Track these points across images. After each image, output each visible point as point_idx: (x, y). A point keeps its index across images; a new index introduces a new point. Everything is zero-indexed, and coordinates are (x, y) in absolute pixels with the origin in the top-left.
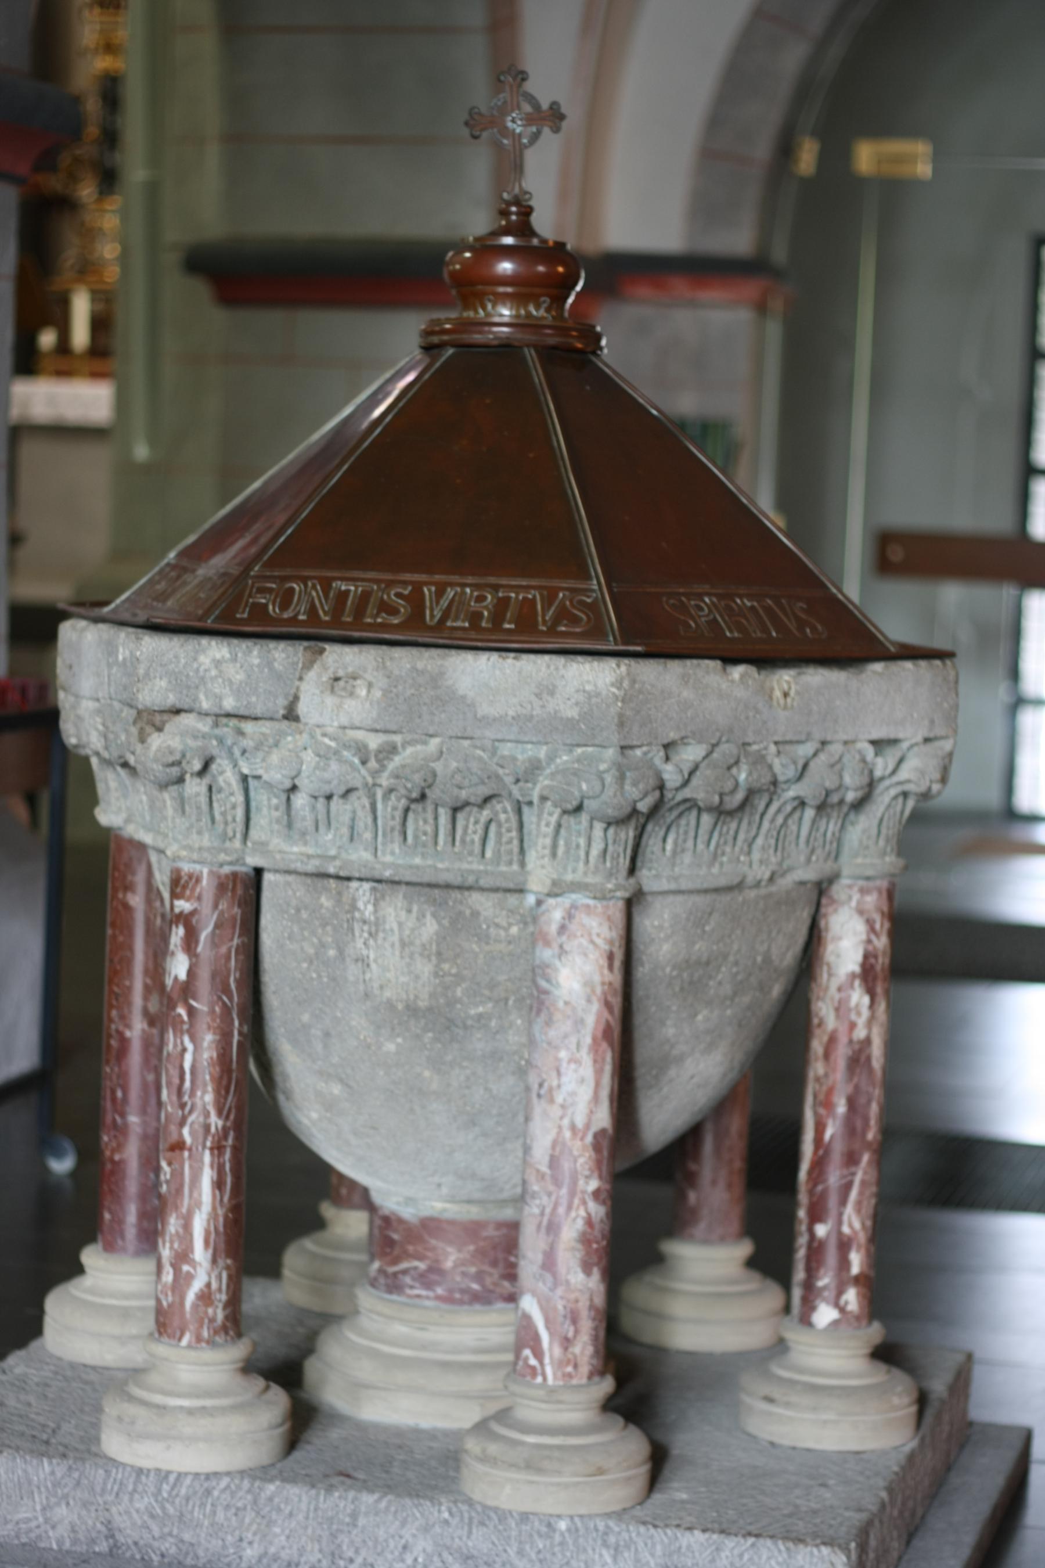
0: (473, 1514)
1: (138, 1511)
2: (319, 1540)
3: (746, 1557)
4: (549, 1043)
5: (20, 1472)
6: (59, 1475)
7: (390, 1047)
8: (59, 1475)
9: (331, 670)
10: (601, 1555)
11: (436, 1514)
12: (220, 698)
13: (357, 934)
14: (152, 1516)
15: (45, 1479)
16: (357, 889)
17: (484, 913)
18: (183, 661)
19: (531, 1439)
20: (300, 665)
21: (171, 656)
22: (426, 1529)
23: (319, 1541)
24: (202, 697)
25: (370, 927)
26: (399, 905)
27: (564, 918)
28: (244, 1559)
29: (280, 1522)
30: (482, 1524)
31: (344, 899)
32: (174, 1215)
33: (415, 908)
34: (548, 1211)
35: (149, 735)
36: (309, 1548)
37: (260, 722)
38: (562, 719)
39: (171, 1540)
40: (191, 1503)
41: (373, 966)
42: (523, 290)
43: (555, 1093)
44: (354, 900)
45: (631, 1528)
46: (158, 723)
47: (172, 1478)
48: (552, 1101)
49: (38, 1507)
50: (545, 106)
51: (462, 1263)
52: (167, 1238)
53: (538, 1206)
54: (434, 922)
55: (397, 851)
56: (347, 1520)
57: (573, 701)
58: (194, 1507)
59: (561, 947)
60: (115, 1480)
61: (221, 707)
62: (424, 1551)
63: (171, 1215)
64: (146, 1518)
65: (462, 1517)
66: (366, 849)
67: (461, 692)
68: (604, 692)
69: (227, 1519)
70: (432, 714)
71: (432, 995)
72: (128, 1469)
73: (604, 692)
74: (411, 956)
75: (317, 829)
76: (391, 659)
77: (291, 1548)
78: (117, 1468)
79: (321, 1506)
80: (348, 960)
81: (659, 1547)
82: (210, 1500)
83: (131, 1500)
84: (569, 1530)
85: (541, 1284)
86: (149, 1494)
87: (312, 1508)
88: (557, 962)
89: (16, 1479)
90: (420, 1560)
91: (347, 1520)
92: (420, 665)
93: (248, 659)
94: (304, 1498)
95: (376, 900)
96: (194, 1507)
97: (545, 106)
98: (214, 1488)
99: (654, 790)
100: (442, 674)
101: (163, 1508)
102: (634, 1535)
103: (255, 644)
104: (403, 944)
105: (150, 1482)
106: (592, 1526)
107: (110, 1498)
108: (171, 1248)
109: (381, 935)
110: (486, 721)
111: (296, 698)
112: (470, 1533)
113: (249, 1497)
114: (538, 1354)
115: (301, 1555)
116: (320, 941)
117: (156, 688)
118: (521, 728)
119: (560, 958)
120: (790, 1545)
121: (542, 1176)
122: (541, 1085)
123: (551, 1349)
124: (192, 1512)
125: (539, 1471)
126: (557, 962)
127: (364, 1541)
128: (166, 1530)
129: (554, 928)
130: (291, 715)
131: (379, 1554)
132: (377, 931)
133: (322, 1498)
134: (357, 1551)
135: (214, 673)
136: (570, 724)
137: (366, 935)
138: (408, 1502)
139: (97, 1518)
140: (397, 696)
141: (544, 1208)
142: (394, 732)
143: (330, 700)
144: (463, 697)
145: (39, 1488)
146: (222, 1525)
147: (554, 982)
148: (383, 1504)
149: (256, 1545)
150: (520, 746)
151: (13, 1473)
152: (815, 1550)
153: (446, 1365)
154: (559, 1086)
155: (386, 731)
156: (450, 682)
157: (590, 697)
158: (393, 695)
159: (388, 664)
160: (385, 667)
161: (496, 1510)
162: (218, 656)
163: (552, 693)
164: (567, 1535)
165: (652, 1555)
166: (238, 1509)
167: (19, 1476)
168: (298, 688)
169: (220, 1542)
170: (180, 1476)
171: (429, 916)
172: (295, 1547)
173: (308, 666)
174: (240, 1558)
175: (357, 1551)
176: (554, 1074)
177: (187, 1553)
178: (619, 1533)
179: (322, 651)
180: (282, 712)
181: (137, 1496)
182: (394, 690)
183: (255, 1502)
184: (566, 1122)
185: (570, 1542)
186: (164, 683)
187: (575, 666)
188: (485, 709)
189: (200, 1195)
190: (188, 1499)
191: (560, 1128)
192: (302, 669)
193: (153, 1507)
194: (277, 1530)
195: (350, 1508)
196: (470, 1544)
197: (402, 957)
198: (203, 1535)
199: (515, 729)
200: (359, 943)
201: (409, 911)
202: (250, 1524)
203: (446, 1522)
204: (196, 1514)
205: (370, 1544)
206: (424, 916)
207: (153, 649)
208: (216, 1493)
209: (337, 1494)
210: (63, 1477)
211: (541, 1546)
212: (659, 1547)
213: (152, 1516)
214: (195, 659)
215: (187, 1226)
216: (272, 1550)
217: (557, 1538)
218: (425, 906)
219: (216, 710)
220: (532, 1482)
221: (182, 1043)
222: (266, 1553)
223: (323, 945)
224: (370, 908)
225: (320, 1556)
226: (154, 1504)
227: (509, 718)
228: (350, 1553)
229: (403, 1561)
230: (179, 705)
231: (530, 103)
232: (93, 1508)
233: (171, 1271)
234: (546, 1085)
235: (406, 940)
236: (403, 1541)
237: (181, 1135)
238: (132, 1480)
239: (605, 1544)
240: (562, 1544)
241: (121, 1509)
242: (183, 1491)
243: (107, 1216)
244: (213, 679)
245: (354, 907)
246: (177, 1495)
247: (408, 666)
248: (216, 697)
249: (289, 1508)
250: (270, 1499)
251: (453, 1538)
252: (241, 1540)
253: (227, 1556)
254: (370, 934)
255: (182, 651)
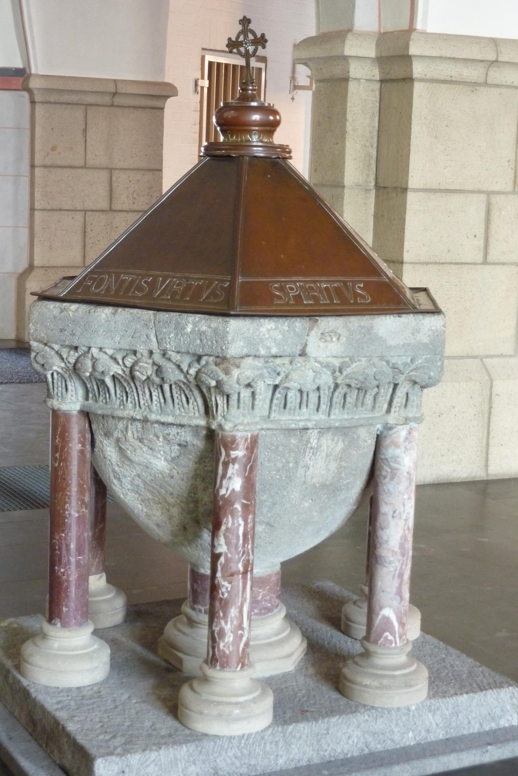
0: (378, 713)
1: (229, 757)
2: (312, 745)
3: (482, 699)
4: (399, 492)
5: (172, 756)
6: (191, 751)
7: (307, 505)
8: (191, 751)
9: (322, 329)
10: (428, 716)
11: (362, 718)
12: (269, 348)
13: (307, 454)
14: (236, 757)
15: (184, 755)
16: (311, 433)
17: (362, 436)
18: (251, 331)
19: (397, 673)
20: (308, 329)
21: (245, 329)
22: (358, 726)
23: (312, 746)
24: (261, 349)
25: (314, 450)
26: (329, 438)
27: (407, 434)
28: (279, 764)
29: (295, 742)
30: (382, 717)
31: (304, 439)
32: (234, 608)
33: (336, 438)
34: (398, 568)
35: (232, 370)
36: (308, 751)
37: (283, 358)
38: (422, 343)
39: (245, 766)
40: (255, 745)
41: (311, 468)
42: (247, 128)
43: (402, 515)
44: (309, 438)
45: (440, 700)
46: (238, 364)
47: (245, 737)
48: (401, 518)
49: (180, 770)
50: (259, 36)
51: (264, 596)
52: (229, 619)
53: (393, 567)
54: (342, 443)
55: (337, 413)
56: (325, 732)
57: (427, 335)
58: (256, 747)
59: (405, 447)
60: (219, 745)
61: (270, 353)
62: (357, 736)
63: (231, 608)
64: (233, 759)
65: (373, 716)
66: (323, 414)
67: (380, 335)
68: (440, 330)
69: (271, 748)
70: (368, 347)
71: (333, 478)
72: (225, 738)
73: (440, 330)
74: (329, 462)
75: (300, 407)
76: (350, 322)
77: (300, 753)
78: (220, 739)
79: (313, 729)
80: (299, 467)
81: (450, 705)
82: (263, 742)
83: (226, 753)
84: (416, 709)
85: (395, 602)
86: (235, 747)
87: (310, 731)
88: (404, 455)
89: (169, 759)
90: (355, 741)
91: (325, 732)
92: (362, 324)
93: (283, 327)
94: (306, 727)
95: (319, 437)
96: (256, 747)
97: (259, 36)
98: (265, 735)
99: (87, 347)
100: (372, 327)
101: (242, 753)
102: (441, 703)
103: (287, 320)
104: (327, 456)
105: (235, 742)
106: (425, 704)
107: (215, 755)
108: (231, 624)
109: (318, 453)
110: (390, 348)
111: (306, 345)
112: (376, 722)
113: (282, 735)
114: (393, 634)
115: (304, 755)
116: (286, 460)
117: (238, 346)
118: (406, 349)
119: (405, 453)
120: (498, 690)
121: (394, 553)
122: (394, 512)
123: (399, 630)
124: (255, 750)
125: (411, 686)
126: (404, 455)
127: (332, 740)
128: (242, 762)
129: (402, 439)
130: (303, 354)
131: (338, 744)
132: (316, 452)
133: (314, 725)
134: (329, 745)
135: (267, 336)
136: (426, 345)
137: (311, 454)
138: (351, 716)
139: (209, 766)
140: (353, 339)
141: (396, 567)
142: (345, 357)
143: (322, 345)
144: (381, 337)
145: (181, 760)
146: (269, 752)
147: (402, 464)
148: (340, 721)
149: (284, 757)
150: (400, 358)
151: (168, 757)
152: (507, 689)
153: (270, 645)
154: (404, 511)
155: (342, 357)
156: (375, 331)
157: (434, 333)
158: (350, 339)
159: (348, 324)
160: (347, 326)
161: (386, 709)
162: (269, 327)
163: (418, 332)
164: (415, 711)
165: (447, 710)
166: (276, 742)
167: (171, 758)
168: (307, 340)
169: (268, 760)
170: (249, 735)
171: (340, 442)
172: (302, 752)
173: (311, 329)
174: (277, 764)
175: (329, 745)
176: (402, 506)
177: (252, 770)
178: (435, 704)
179: (317, 321)
180: (298, 352)
181: (229, 750)
182: (351, 337)
183: (284, 736)
184: (406, 526)
185: (416, 714)
186: (242, 343)
187: (428, 318)
188: (391, 342)
189: (246, 595)
190: (253, 744)
191: (404, 530)
192: (309, 330)
193: (237, 753)
194: (294, 746)
195: (326, 726)
196: (376, 727)
197: (325, 462)
198: (260, 759)
199: (403, 350)
200: (307, 459)
201: (333, 440)
202: (281, 748)
203: (367, 720)
204: (257, 750)
205: (334, 740)
206: (338, 442)
207: (236, 326)
208: (266, 737)
209: (320, 721)
210: (193, 751)
211: (404, 719)
212: (450, 705)
213: (236, 757)
214: (258, 330)
215: (241, 612)
216: (292, 756)
217: (411, 714)
218: (340, 437)
219: (268, 354)
220: (408, 692)
221: (238, 522)
222: (289, 759)
223: (288, 462)
224: (316, 441)
225: (312, 752)
226: (237, 751)
227: (401, 345)
228: (326, 748)
229: (348, 743)
230: (249, 354)
231: (252, 34)
232: (207, 762)
233: (232, 635)
234: (397, 511)
235: (329, 454)
236: (348, 735)
237: (238, 567)
238: (227, 743)
239: (430, 711)
240: (414, 716)
241: (221, 758)
242: (251, 741)
243: (64, 609)
244: (267, 339)
245: (308, 442)
246: (248, 744)
247: (357, 325)
248: (267, 348)
249: (299, 734)
250: (291, 732)
251: (369, 727)
252: (277, 756)
253: (271, 766)
254: (313, 454)
255: (251, 326)
